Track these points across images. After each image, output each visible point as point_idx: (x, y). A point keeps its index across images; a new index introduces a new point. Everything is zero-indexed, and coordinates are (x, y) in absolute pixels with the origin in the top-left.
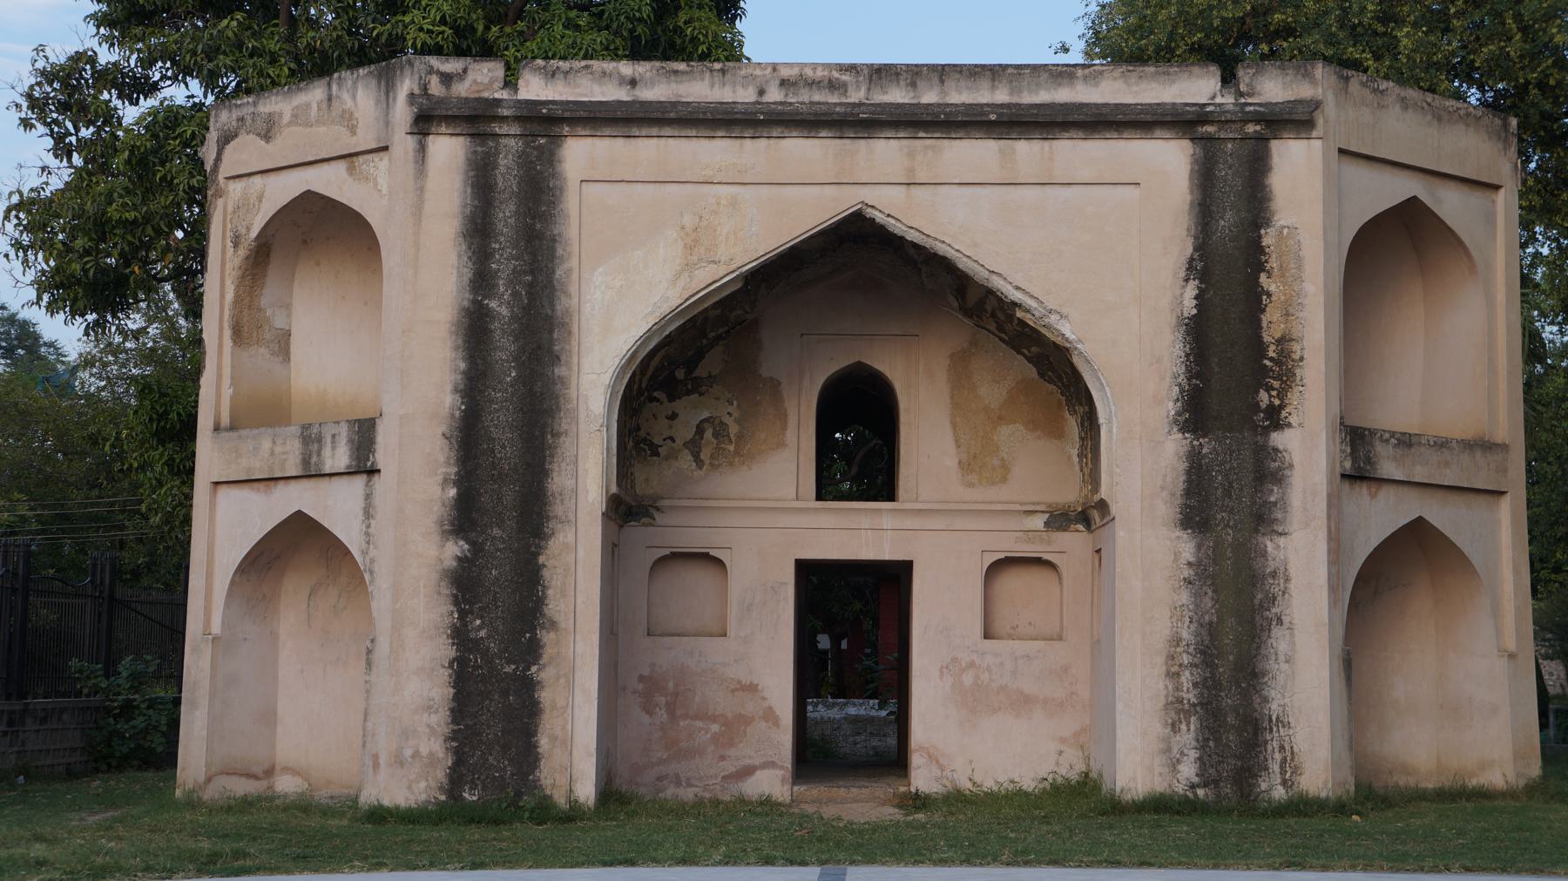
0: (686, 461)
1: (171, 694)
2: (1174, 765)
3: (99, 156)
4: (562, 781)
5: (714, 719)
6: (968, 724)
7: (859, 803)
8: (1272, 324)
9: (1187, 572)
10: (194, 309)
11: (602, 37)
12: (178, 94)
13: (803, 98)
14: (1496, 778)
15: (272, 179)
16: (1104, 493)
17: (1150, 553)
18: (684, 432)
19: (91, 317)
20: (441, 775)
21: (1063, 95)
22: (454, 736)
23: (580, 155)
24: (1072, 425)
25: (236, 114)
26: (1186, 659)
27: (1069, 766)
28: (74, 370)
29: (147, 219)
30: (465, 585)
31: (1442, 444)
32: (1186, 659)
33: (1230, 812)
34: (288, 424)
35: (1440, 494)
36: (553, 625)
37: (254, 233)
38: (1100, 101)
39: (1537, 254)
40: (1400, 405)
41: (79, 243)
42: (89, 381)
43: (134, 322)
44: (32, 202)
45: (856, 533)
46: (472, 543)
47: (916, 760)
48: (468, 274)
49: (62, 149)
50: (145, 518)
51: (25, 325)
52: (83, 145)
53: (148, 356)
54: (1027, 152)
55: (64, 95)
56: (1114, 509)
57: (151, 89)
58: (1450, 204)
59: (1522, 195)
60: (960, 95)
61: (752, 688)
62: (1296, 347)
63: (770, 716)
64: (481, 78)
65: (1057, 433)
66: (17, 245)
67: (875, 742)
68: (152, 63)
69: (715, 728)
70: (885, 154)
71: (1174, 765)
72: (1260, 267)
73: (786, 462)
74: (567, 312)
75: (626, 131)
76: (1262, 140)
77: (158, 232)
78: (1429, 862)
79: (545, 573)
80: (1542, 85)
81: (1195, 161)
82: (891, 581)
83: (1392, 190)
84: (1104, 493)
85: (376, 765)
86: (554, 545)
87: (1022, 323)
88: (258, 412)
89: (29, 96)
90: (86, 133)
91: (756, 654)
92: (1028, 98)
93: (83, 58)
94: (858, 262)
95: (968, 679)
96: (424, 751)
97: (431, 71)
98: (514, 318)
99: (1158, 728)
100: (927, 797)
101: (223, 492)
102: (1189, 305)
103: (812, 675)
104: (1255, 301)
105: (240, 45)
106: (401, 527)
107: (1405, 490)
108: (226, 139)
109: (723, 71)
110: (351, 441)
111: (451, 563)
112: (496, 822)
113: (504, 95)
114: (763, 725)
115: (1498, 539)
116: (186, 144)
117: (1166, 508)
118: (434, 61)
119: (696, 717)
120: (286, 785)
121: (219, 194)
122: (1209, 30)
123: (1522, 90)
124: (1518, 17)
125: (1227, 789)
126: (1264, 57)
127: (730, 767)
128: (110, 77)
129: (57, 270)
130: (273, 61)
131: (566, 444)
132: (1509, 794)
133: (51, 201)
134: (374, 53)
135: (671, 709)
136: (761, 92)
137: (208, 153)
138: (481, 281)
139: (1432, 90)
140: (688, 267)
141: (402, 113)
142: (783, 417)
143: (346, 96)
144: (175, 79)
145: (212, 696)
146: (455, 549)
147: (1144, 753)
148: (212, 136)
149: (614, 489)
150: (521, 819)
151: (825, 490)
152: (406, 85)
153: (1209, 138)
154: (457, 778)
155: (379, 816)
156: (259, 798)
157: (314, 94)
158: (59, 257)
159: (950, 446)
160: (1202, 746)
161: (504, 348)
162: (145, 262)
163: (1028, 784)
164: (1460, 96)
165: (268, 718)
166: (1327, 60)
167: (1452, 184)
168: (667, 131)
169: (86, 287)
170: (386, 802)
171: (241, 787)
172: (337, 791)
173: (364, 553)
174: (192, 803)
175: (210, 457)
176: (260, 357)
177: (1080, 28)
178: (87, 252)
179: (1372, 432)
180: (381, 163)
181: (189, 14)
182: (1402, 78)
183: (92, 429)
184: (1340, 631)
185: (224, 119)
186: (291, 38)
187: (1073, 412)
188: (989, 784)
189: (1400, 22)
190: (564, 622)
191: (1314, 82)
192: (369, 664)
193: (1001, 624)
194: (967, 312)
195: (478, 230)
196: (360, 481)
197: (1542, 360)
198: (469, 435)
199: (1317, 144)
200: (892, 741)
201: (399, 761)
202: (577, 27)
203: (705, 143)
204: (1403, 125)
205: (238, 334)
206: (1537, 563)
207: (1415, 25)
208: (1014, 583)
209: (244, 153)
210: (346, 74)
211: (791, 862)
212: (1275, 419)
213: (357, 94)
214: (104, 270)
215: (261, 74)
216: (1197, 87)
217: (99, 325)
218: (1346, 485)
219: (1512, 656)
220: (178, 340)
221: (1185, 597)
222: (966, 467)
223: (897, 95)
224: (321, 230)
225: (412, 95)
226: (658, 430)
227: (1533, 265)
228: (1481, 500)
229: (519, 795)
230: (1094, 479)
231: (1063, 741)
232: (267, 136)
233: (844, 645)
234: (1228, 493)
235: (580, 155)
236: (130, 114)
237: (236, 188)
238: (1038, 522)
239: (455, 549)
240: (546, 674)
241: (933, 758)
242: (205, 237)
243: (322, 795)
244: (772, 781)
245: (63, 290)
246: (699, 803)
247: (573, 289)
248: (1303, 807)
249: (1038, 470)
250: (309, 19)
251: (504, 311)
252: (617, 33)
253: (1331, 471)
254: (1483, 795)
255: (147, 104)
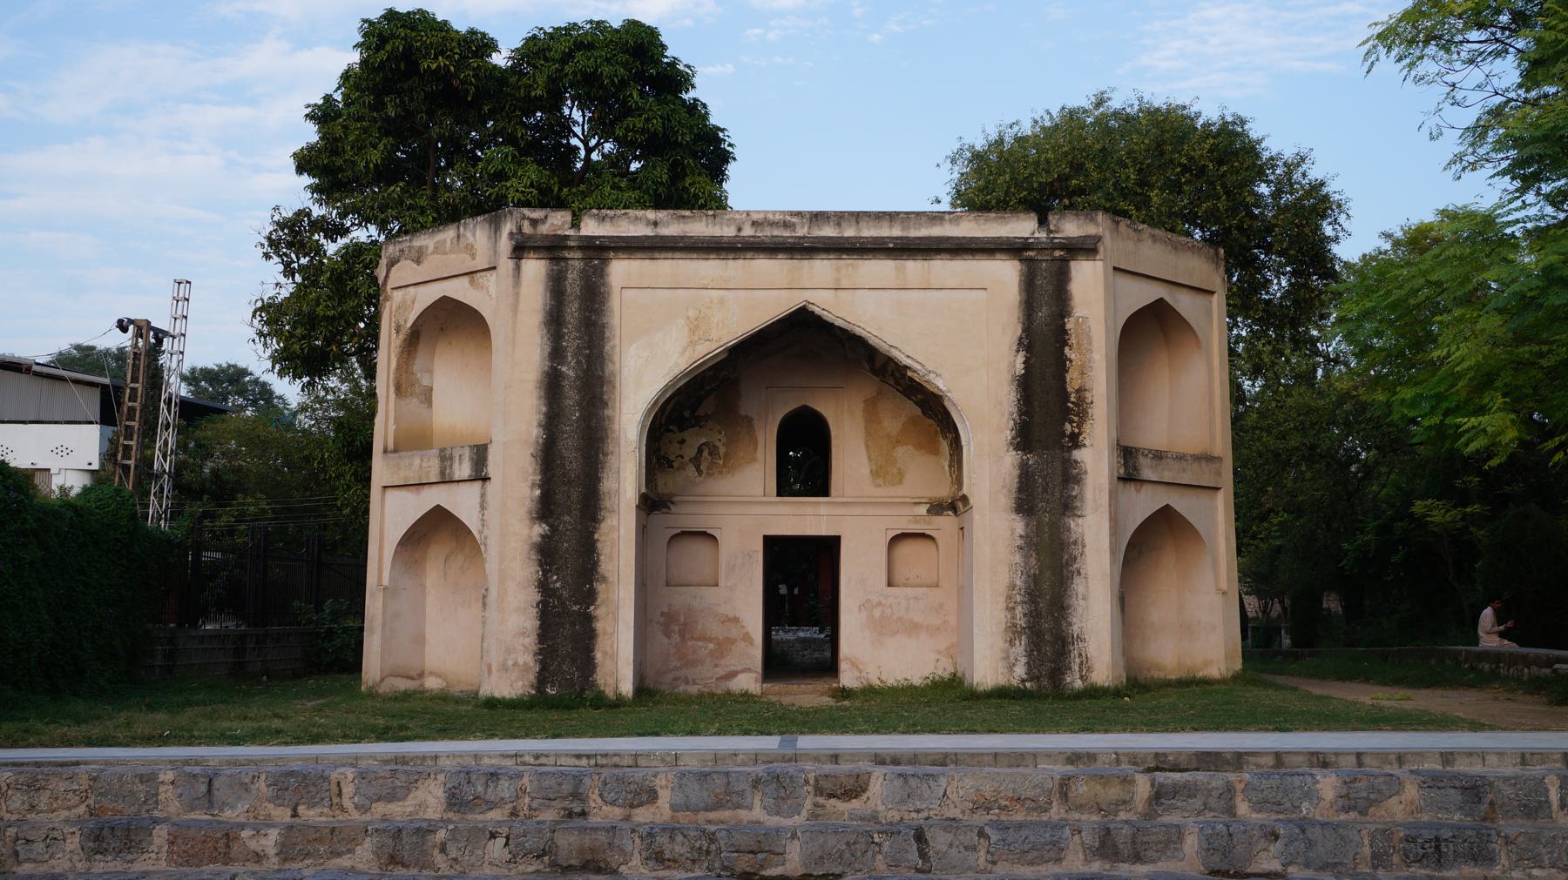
0: (691, 471)
1: (357, 624)
2: (1011, 667)
3: (311, 275)
4: (611, 681)
5: (710, 640)
6: (879, 641)
7: (806, 695)
8: (1073, 380)
9: (1020, 542)
10: (371, 373)
11: (635, 194)
12: (363, 234)
13: (766, 233)
14: (1214, 672)
15: (421, 289)
16: (965, 490)
17: (995, 529)
18: (690, 452)
19: (306, 379)
20: (532, 677)
21: (937, 231)
22: (540, 652)
23: (620, 270)
24: (945, 446)
25: (398, 247)
26: (1019, 598)
27: (944, 670)
28: (295, 414)
29: (341, 315)
30: (546, 553)
31: (1181, 458)
32: (1019, 598)
33: (1047, 696)
34: (431, 448)
35: (1180, 490)
36: (604, 579)
37: (409, 324)
38: (960, 234)
39: (1239, 336)
40: (1155, 432)
41: (298, 331)
42: (304, 421)
43: (333, 382)
44: (270, 305)
45: (803, 518)
46: (551, 526)
47: (844, 666)
48: (547, 349)
49: (289, 272)
50: (340, 509)
51: (264, 384)
52: (302, 269)
53: (341, 404)
54: (914, 268)
55: (291, 237)
56: (972, 501)
57: (344, 231)
58: (1184, 304)
59: (1228, 298)
60: (869, 231)
61: (736, 620)
62: (1088, 395)
63: (747, 638)
64: (557, 222)
65: (935, 451)
66: (260, 334)
67: (817, 655)
68: (346, 216)
69: (711, 646)
70: (821, 269)
71: (1011, 667)
72: (1065, 343)
73: (757, 472)
74: (613, 373)
75: (649, 255)
76: (1065, 262)
77: (348, 324)
78: (1172, 726)
79: (599, 545)
80: (1239, 228)
81: (1022, 275)
82: (825, 551)
83: (1146, 294)
84: (965, 490)
85: (490, 671)
86: (604, 527)
87: (911, 379)
88: (411, 441)
89: (269, 238)
90: (304, 261)
91: (739, 598)
92: (913, 233)
93: (303, 213)
94: (805, 341)
95: (877, 613)
96: (521, 661)
97: (524, 217)
98: (578, 377)
99: (1001, 644)
100: (851, 690)
101: (389, 492)
102: (1020, 368)
103: (775, 612)
104: (1061, 365)
105: (401, 202)
106: (505, 516)
107: (1157, 487)
108: (392, 263)
109: (714, 216)
110: (471, 459)
111: (537, 539)
112: (569, 708)
113: (571, 232)
114: (742, 644)
115: (1216, 518)
116: (366, 267)
117: (1006, 500)
118: (526, 211)
119: (699, 639)
120: (432, 683)
121: (387, 299)
122: (1031, 190)
123: (1227, 231)
124: (1224, 185)
125: (1045, 682)
126: (1066, 208)
127: (721, 672)
128: (320, 225)
129: (284, 349)
130: (423, 213)
131: (612, 460)
132: (1222, 681)
133: (281, 304)
134: (487, 206)
135: (682, 634)
136: (739, 230)
137: (381, 272)
138: (556, 354)
139: (1172, 230)
140: (692, 343)
141: (505, 244)
142: (755, 443)
143: (469, 235)
144: (360, 225)
145: (384, 626)
146: (539, 529)
147: (992, 661)
148: (383, 262)
149: (644, 490)
150: (584, 706)
151: (784, 489)
152: (508, 227)
153: (1031, 260)
154: (542, 679)
155: (492, 703)
156: (415, 692)
157: (449, 234)
158: (286, 341)
159: (865, 460)
160: (1029, 655)
161: (571, 397)
162: (340, 343)
163: (917, 681)
164: (1189, 234)
165: (420, 640)
166: (1106, 210)
167: (1185, 290)
168: (678, 255)
169: (302, 360)
170: (497, 695)
171: (403, 685)
172: (465, 688)
173: (481, 532)
174: (372, 694)
175: (381, 471)
176: (413, 403)
177: (948, 188)
178: (304, 337)
179: (1137, 450)
180: (491, 278)
181: (369, 184)
182: (1152, 222)
183: (306, 453)
184: (1117, 579)
185: (391, 250)
186: (434, 198)
187: (945, 438)
188: (891, 682)
189: (1151, 187)
190: (612, 577)
191: (1097, 225)
192: (484, 604)
193: (899, 576)
194: (875, 372)
195: (554, 321)
196: (478, 485)
197: (1243, 403)
198: (548, 455)
199: (1100, 264)
200: (828, 654)
201: (504, 668)
202: (620, 189)
203: (703, 263)
204: (1153, 252)
205: (399, 390)
206: (1240, 534)
207: (1162, 189)
208: (906, 549)
209: (404, 272)
210: (469, 221)
211: (762, 733)
212: (1075, 441)
213: (477, 233)
214: (313, 349)
215: (414, 221)
216: (1023, 227)
217: (311, 384)
218: (1121, 484)
219: (1224, 593)
220: (360, 394)
221: (1018, 558)
222: (875, 474)
223: (828, 231)
224: (453, 321)
225: (511, 234)
226: (673, 450)
227: (1237, 343)
228: (1205, 495)
229: (583, 690)
230: (959, 481)
231: (939, 652)
232: (418, 262)
233: (796, 591)
234: (1045, 490)
235: (620, 270)
236: (331, 248)
237: (398, 295)
238: (923, 510)
239: (539, 529)
240: (599, 611)
241: (854, 665)
242: (378, 327)
243: (455, 691)
244: (749, 681)
245: (288, 362)
246: (701, 696)
247: (616, 358)
248: (1093, 693)
249: (922, 476)
250: (446, 185)
251: (571, 373)
252: (646, 192)
253: (1111, 474)
254: (1206, 682)
255: (342, 242)
